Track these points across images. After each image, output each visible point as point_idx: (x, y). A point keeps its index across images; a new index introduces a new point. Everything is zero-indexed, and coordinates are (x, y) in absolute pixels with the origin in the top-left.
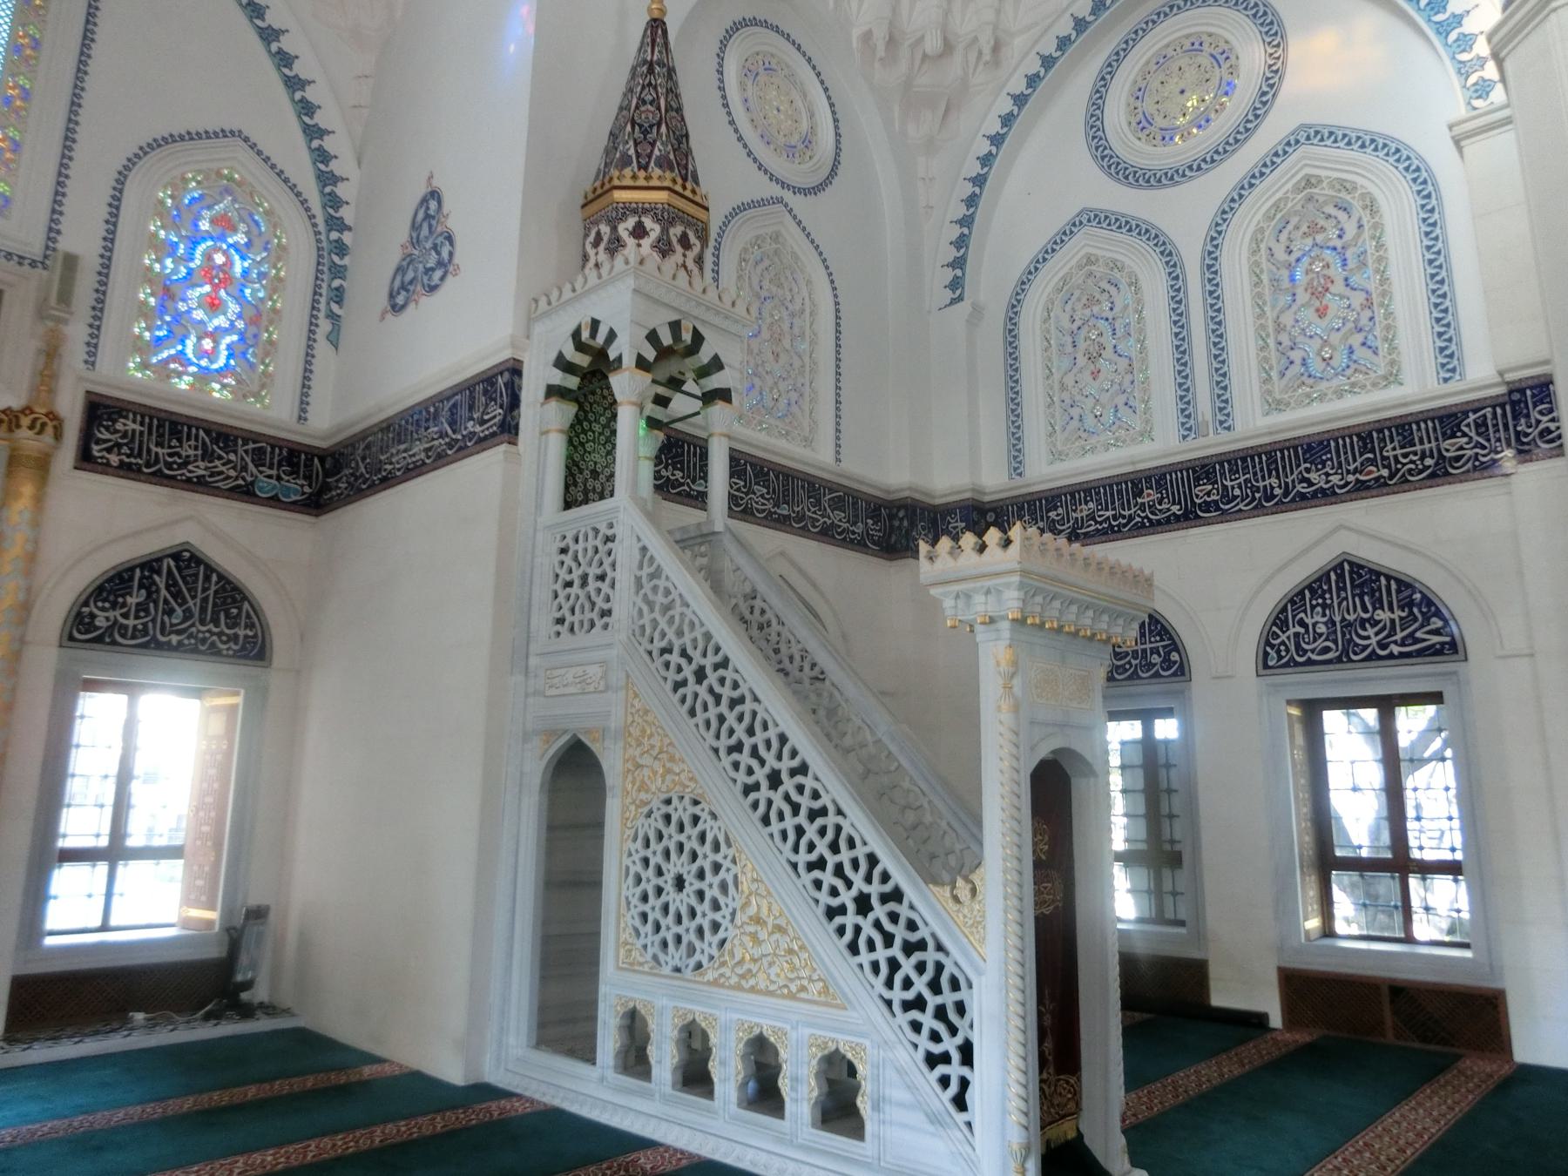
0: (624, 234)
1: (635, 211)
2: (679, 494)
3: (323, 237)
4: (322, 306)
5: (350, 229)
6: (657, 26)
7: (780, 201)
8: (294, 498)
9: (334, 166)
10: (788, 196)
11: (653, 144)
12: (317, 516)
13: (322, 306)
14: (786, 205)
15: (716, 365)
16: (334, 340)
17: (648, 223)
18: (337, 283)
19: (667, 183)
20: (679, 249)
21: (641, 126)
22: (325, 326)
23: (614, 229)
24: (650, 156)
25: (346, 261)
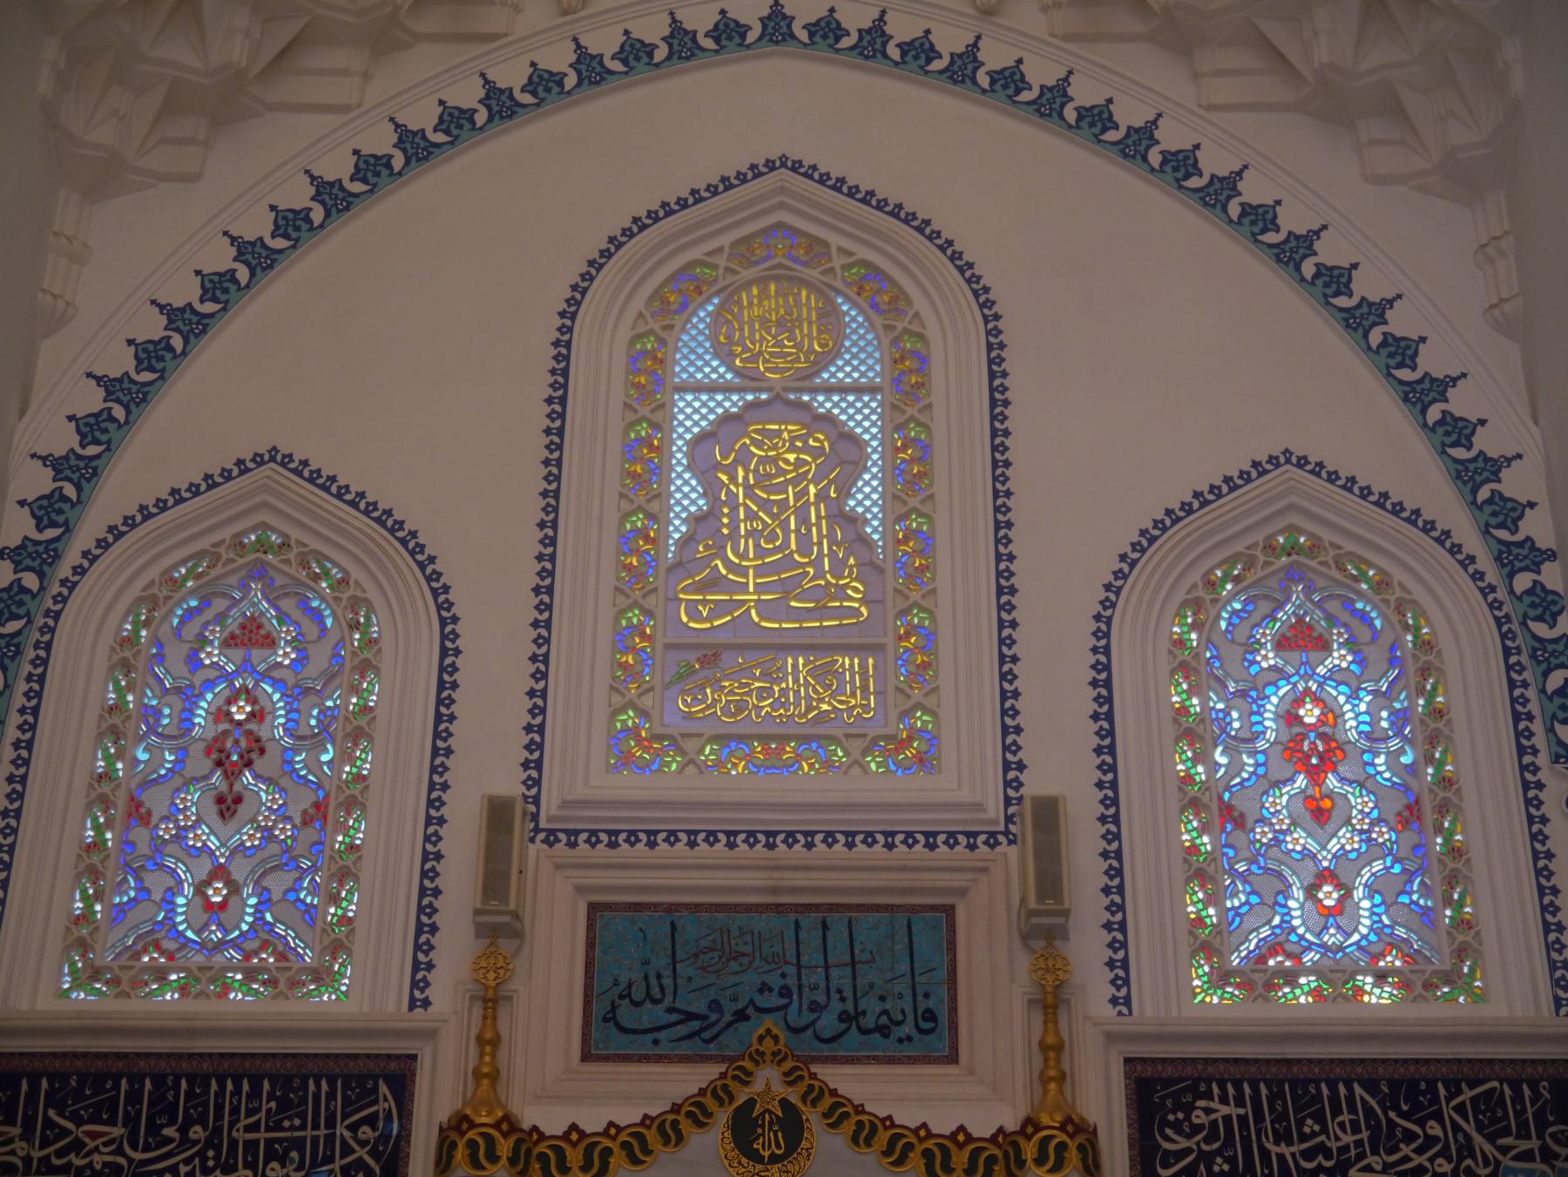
3: (1501, 594)
4: (1540, 740)
5: (1552, 555)
9: (1486, 442)
13: (1540, 740)
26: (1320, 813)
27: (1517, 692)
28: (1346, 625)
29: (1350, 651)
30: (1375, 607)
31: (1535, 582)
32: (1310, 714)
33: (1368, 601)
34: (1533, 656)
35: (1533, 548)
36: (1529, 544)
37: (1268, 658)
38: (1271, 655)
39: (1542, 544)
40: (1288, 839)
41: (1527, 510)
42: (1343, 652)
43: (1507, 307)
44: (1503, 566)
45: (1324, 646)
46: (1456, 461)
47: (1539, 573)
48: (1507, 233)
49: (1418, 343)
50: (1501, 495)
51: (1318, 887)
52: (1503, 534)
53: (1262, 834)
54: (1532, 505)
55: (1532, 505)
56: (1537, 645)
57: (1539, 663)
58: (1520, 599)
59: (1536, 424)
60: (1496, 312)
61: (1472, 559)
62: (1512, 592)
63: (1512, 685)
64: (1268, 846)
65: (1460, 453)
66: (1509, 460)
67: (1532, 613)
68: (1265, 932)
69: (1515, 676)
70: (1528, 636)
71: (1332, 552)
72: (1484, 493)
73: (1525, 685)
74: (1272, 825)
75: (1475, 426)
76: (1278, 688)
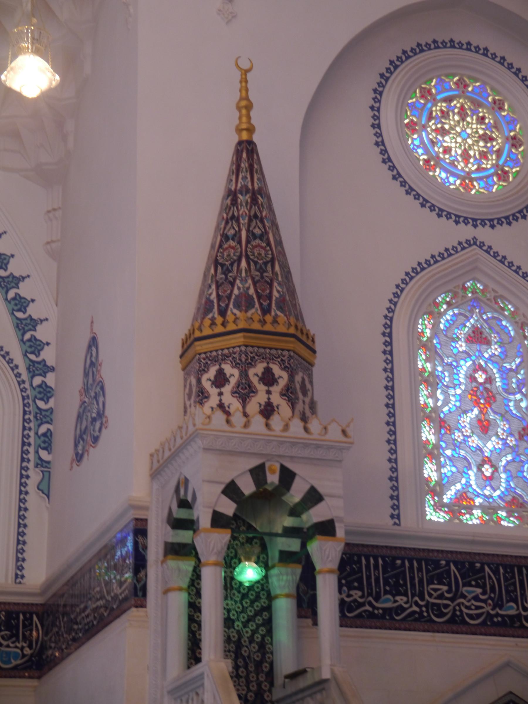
0: (207, 385)
1: (215, 360)
2: (360, 616)
3: (27, 385)
4: (31, 456)
5: (52, 369)
6: (247, 152)
7: (472, 242)
8: (14, 663)
9: (33, 311)
10: (483, 234)
11: (232, 284)
12: (39, 677)
13: (31, 456)
14: (481, 245)
15: (314, 497)
16: (45, 490)
17: (228, 369)
18: (43, 429)
19: (242, 325)
20: (261, 388)
21: (222, 265)
22: (35, 476)
23: (199, 381)
24: (229, 297)
25: (51, 403)
26: (484, 427)
27: (26, 432)
28: (498, 333)
29: (500, 347)
30: (511, 325)
31: (43, 382)
32: (481, 377)
33: (508, 322)
34: (36, 417)
35: (45, 365)
36: (43, 363)
37: (462, 346)
38: (464, 344)
39: (49, 363)
40: (469, 440)
41: (46, 347)
42: (496, 347)
43: (54, 245)
44: (30, 372)
45: (488, 342)
46: (17, 318)
47: (45, 377)
48: (60, 208)
49: (10, 257)
50: (35, 337)
51: (482, 465)
52: (32, 357)
53: (458, 436)
54: (48, 344)
55: (48, 344)
56: (38, 411)
57: (37, 420)
58: (34, 389)
59: (57, 305)
60: (49, 247)
61: (17, 367)
62: (31, 385)
63: (24, 428)
64: (460, 443)
65: (20, 315)
66: (41, 321)
67: (39, 396)
68: (459, 486)
69: (26, 424)
70: (35, 406)
71: (493, 294)
72: (27, 336)
73: (30, 429)
74: (462, 432)
75: (29, 302)
76: (466, 362)
